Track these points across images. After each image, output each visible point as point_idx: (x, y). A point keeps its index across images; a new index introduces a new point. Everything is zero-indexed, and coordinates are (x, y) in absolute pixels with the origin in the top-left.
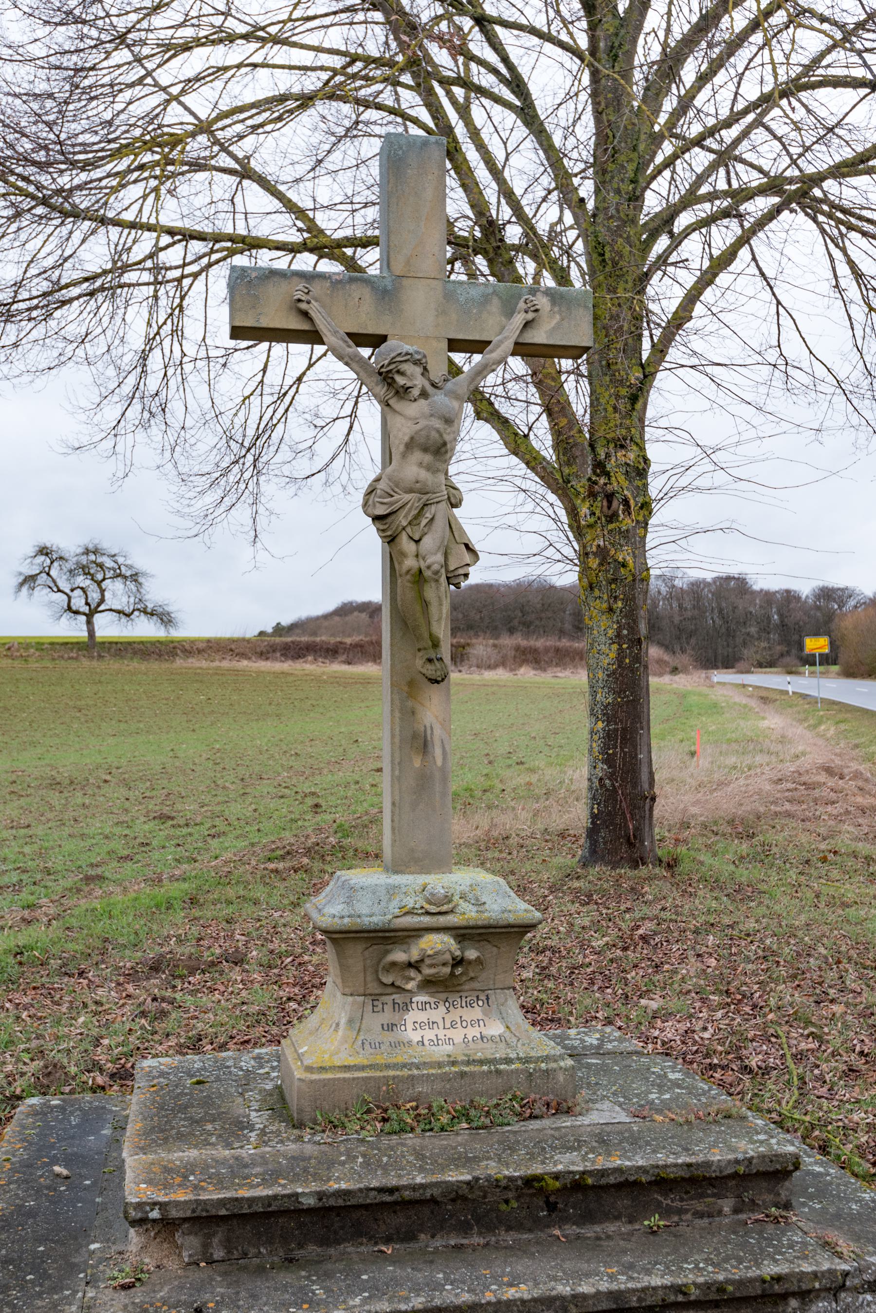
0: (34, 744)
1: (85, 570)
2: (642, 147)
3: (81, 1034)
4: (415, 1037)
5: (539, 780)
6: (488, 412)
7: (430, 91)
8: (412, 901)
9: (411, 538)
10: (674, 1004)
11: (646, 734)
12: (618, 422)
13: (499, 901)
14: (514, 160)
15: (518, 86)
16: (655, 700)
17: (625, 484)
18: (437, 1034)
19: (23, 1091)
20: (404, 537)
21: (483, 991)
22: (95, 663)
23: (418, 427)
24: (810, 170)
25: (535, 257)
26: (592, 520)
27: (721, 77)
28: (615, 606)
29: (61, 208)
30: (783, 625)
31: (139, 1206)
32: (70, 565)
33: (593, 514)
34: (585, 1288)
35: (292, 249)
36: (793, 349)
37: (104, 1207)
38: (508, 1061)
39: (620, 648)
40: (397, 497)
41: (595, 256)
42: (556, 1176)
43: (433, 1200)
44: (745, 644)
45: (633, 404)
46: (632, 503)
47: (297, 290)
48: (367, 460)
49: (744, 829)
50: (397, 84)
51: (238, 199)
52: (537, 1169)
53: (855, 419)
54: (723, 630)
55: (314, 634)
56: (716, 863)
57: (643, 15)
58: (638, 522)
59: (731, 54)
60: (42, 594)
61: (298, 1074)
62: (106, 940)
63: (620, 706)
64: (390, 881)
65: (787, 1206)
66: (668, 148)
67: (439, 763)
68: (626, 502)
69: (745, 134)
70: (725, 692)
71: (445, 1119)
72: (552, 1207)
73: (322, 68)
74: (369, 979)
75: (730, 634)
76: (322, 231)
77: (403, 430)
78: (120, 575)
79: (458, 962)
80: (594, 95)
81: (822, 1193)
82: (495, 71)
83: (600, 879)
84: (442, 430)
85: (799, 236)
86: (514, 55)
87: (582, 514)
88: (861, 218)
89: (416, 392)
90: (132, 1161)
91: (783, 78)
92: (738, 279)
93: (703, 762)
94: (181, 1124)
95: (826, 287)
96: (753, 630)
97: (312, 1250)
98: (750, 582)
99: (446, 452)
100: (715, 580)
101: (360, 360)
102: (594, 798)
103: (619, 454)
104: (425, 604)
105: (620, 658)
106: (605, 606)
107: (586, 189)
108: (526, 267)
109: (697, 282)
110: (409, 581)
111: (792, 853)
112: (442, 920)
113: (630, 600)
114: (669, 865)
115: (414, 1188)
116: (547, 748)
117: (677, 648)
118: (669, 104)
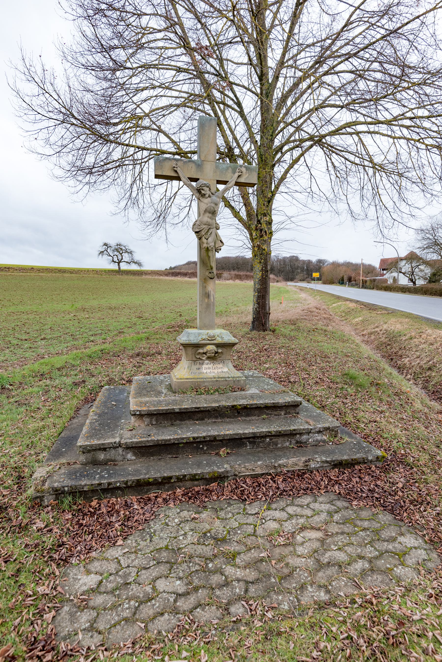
0: (105, 298)
2: (274, 125)
4: (205, 371)
6: (228, 205)
7: (214, 106)
10: (272, 366)
14: (238, 128)
16: (271, 290)
18: (210, 371)
24: (323, 133)
25: (242, 158)
27: (298, 104)
29: (105, 139)
30: (307, 270)
31: (134, 411)
32: (113, 249)
34: (246, 431)
35: (174, 154)
36: (315, 188)
37: (125, 412)
38: (229, 378)
42: (240, 405)
43: (209, 411)
47: (174, 164)
48: (194, 216)
49: (293, 322)
50: (204, 103)
51: (158, 139)
52: (235, 403)
53: (331, 209)
56: (285, 331)
57: (276, 83)
59: (302, 96)
60: (105, 257)
61: (175, 380)
65: (298, 413)
66: (282, 125)
68: (266, 232)
69: (305, 121)
71: (212, 391)
72: (239, 413)
73: (181, 97)
75: (293, 272)
76: (182, 149)
77: (204, 207)
79: (216, 353)
80: (261, 108)
81: (307, 410)
82: (232, 100)
85: (318, 153)
86: (238, 94)
88: (336, 149)
89: (207, 196)
90: (132, 400)
91: (316, 104)
92: (300, 167)
93: (284, 305)
94: (145, 392)
95: (324, 170)
96: (299, 271)
97: (178, 422)
101: (192, 186)
104: (209, 257)
105: (262, 276)
107: (258, 138)
108: (240, 162)
111: (305, 328)
112: (212, 342)
115: (204, 408)
118: (284, 111)
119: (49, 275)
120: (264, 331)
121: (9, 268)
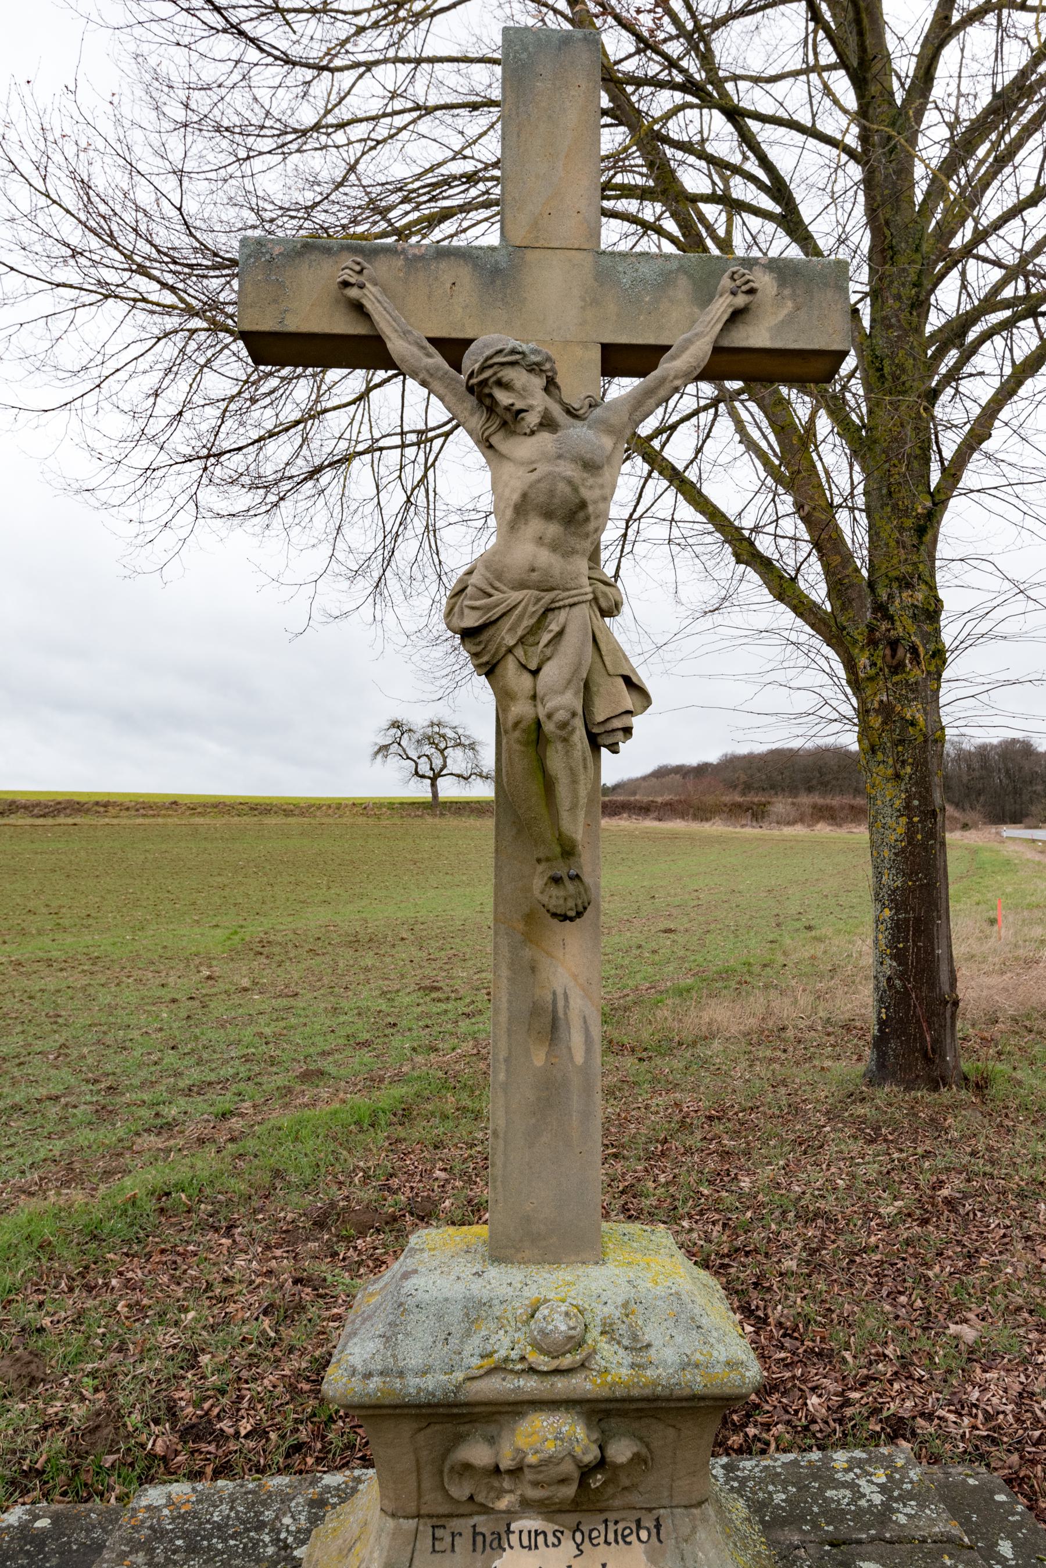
1: (430, 740)
3: (174, 1346)
5: (825, 952)
8: (506, 1342)
9: (524, 667)
10: (1000, 1334)
11: (944, 925)
12: (904, 557)
13: (679, 1339)
15: (779, 190)
17: (912, 629)
19: (48, 1461)
20: (511, 664)
21: (650, 1510)
22: (437, 820)
23: (534, 476)
26: (872, 672)
28: (902, 773)
32: (417, 736)
33: (873, 664)
39: (910, 822)
40: (497, 596)
41: (871, 372)
44: (1031, 802)
45: (920, 537)
46: (921, 649)
54: (1010, 788)
55: (634, 794)
58: (929, 673)
62: (277, 1174)
63: (911, 890)
64: (477, 1288)
67: (579, 1058)
68: (914, 650)
70: (1017, 848)
74: (426, 1484)
75: (1017, 792)
78: (460, 744)
83: (891, 1105)
84: (577, 481)
86: (773, 154)
87: (861, 665)
89: (532, 419)
93: (1005, 932)
98: (1035, 745)
99: (587, 519)
100: (1001, 744)
102: (881, 1000)
103: (904, 595)
104: (549, 785)
105: (910, 831)
106: (890, 771)
109: (997, 393)
110: (519, 742)
112: (561, 1386)
113: (921, 764)
114: (977, 1085)
116: (838, 909)
117: (967, 806)
119: (220, 821)
120: (935, 1084)
121: (106, 805)
